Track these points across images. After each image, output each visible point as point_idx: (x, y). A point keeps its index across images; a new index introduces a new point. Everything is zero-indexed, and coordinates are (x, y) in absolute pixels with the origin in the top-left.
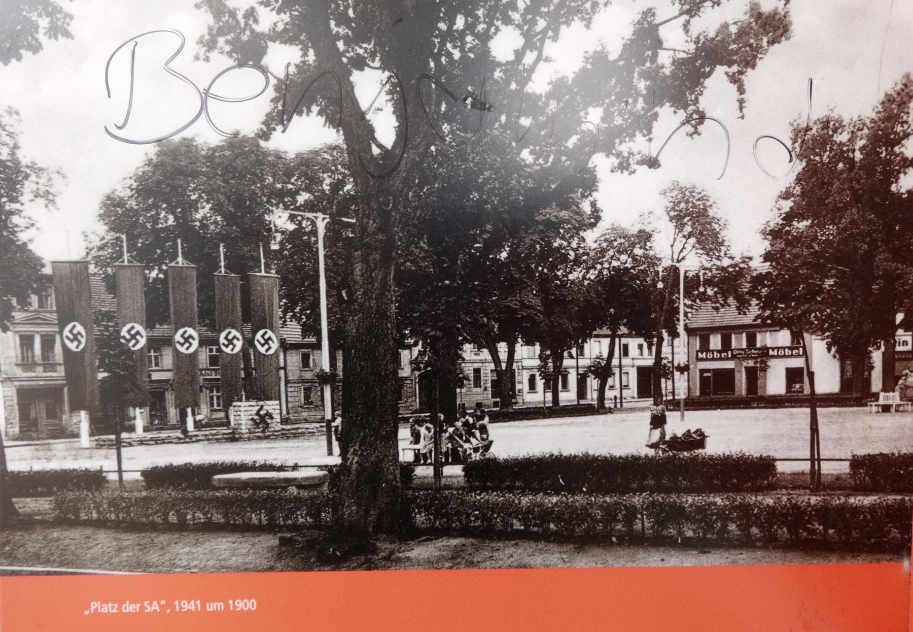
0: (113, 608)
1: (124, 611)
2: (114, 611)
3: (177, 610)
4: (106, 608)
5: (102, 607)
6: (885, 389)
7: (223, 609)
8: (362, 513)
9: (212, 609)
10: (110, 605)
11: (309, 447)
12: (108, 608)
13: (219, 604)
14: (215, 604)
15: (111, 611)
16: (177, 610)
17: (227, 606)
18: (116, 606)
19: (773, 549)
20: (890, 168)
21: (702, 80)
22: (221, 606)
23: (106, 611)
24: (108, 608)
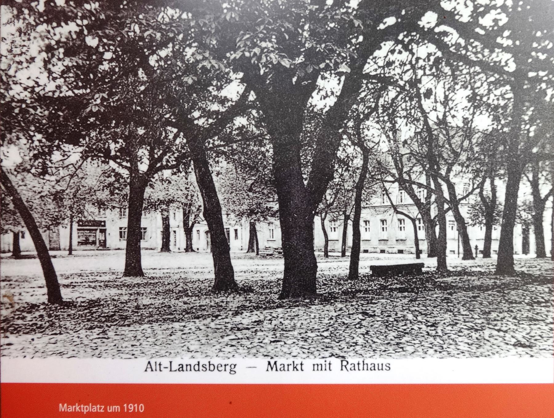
0: (100, 408)
1: (109, 411)
2: (102, 411)
3: (126, 411)
4: (95, 408)
5: (68, 408)
6: (36, 111)
7: (119, 411)
8: (459, 290)
9: (111, 411)
10: (98, 406)
11: (367, 258)
12: (132, 407)
13: (116, 407)
14: (114, 407)
15: (99, 411)
16: (126, 411)
17: (122, 408)
18: (103, 407)
19: (523, 229)
20: (100, 73)
21: (245, 84)
22: (110, 409)
23: (95, 411)
24: (132, 407)
